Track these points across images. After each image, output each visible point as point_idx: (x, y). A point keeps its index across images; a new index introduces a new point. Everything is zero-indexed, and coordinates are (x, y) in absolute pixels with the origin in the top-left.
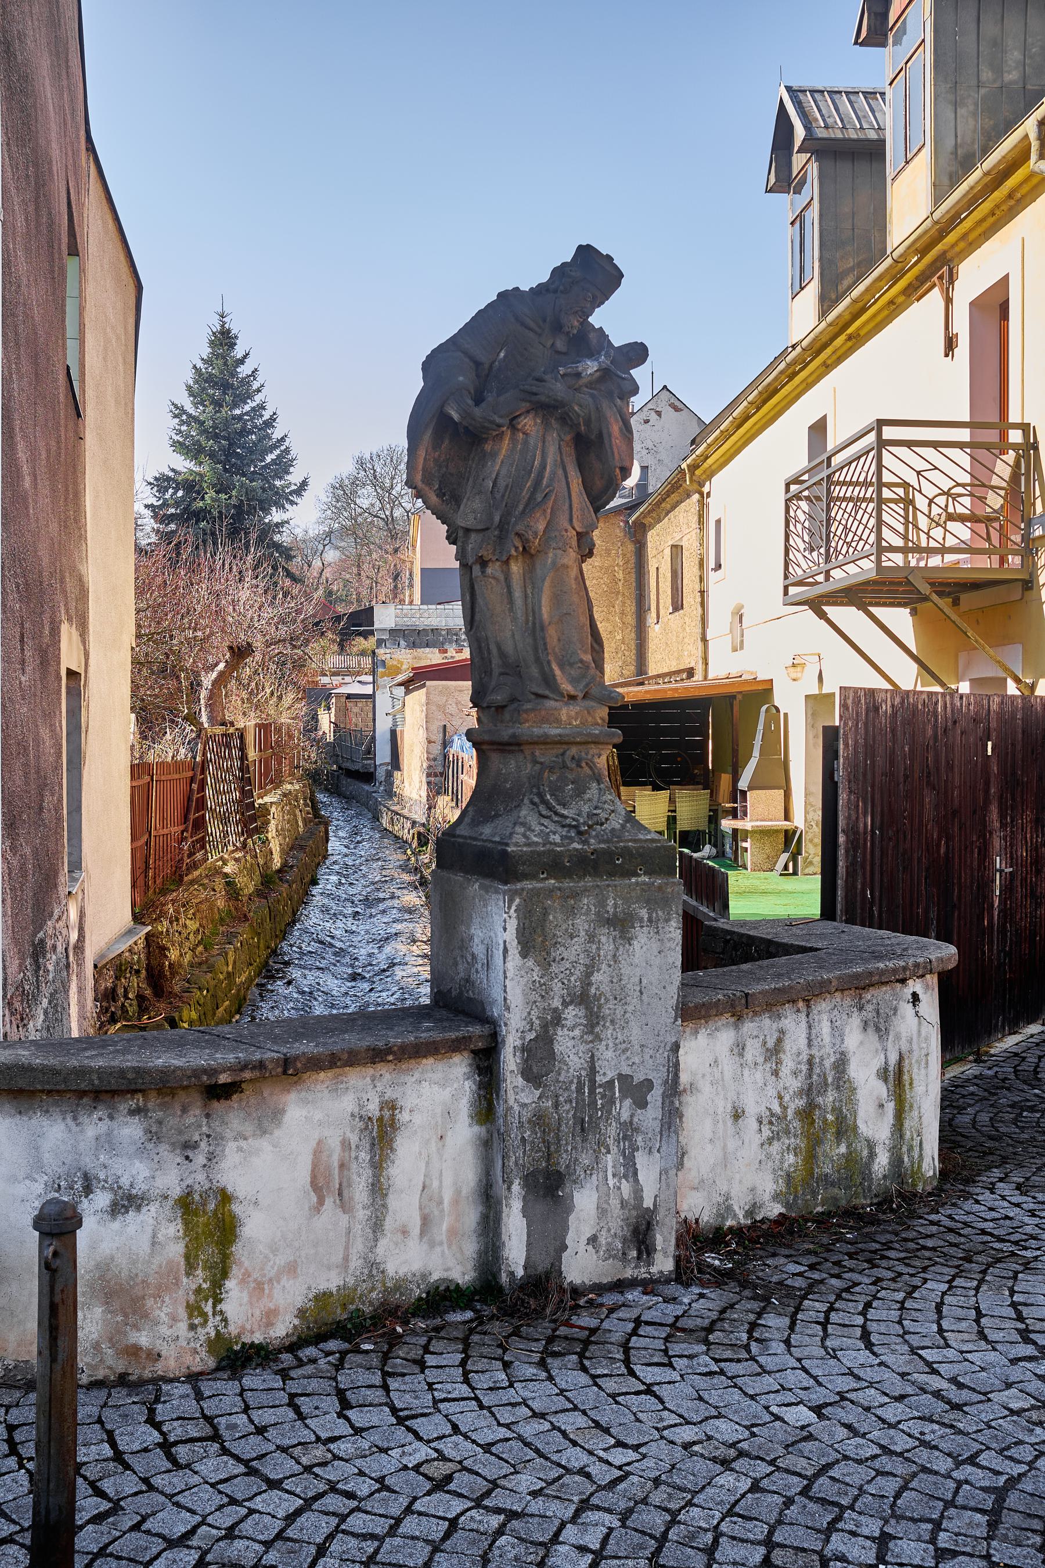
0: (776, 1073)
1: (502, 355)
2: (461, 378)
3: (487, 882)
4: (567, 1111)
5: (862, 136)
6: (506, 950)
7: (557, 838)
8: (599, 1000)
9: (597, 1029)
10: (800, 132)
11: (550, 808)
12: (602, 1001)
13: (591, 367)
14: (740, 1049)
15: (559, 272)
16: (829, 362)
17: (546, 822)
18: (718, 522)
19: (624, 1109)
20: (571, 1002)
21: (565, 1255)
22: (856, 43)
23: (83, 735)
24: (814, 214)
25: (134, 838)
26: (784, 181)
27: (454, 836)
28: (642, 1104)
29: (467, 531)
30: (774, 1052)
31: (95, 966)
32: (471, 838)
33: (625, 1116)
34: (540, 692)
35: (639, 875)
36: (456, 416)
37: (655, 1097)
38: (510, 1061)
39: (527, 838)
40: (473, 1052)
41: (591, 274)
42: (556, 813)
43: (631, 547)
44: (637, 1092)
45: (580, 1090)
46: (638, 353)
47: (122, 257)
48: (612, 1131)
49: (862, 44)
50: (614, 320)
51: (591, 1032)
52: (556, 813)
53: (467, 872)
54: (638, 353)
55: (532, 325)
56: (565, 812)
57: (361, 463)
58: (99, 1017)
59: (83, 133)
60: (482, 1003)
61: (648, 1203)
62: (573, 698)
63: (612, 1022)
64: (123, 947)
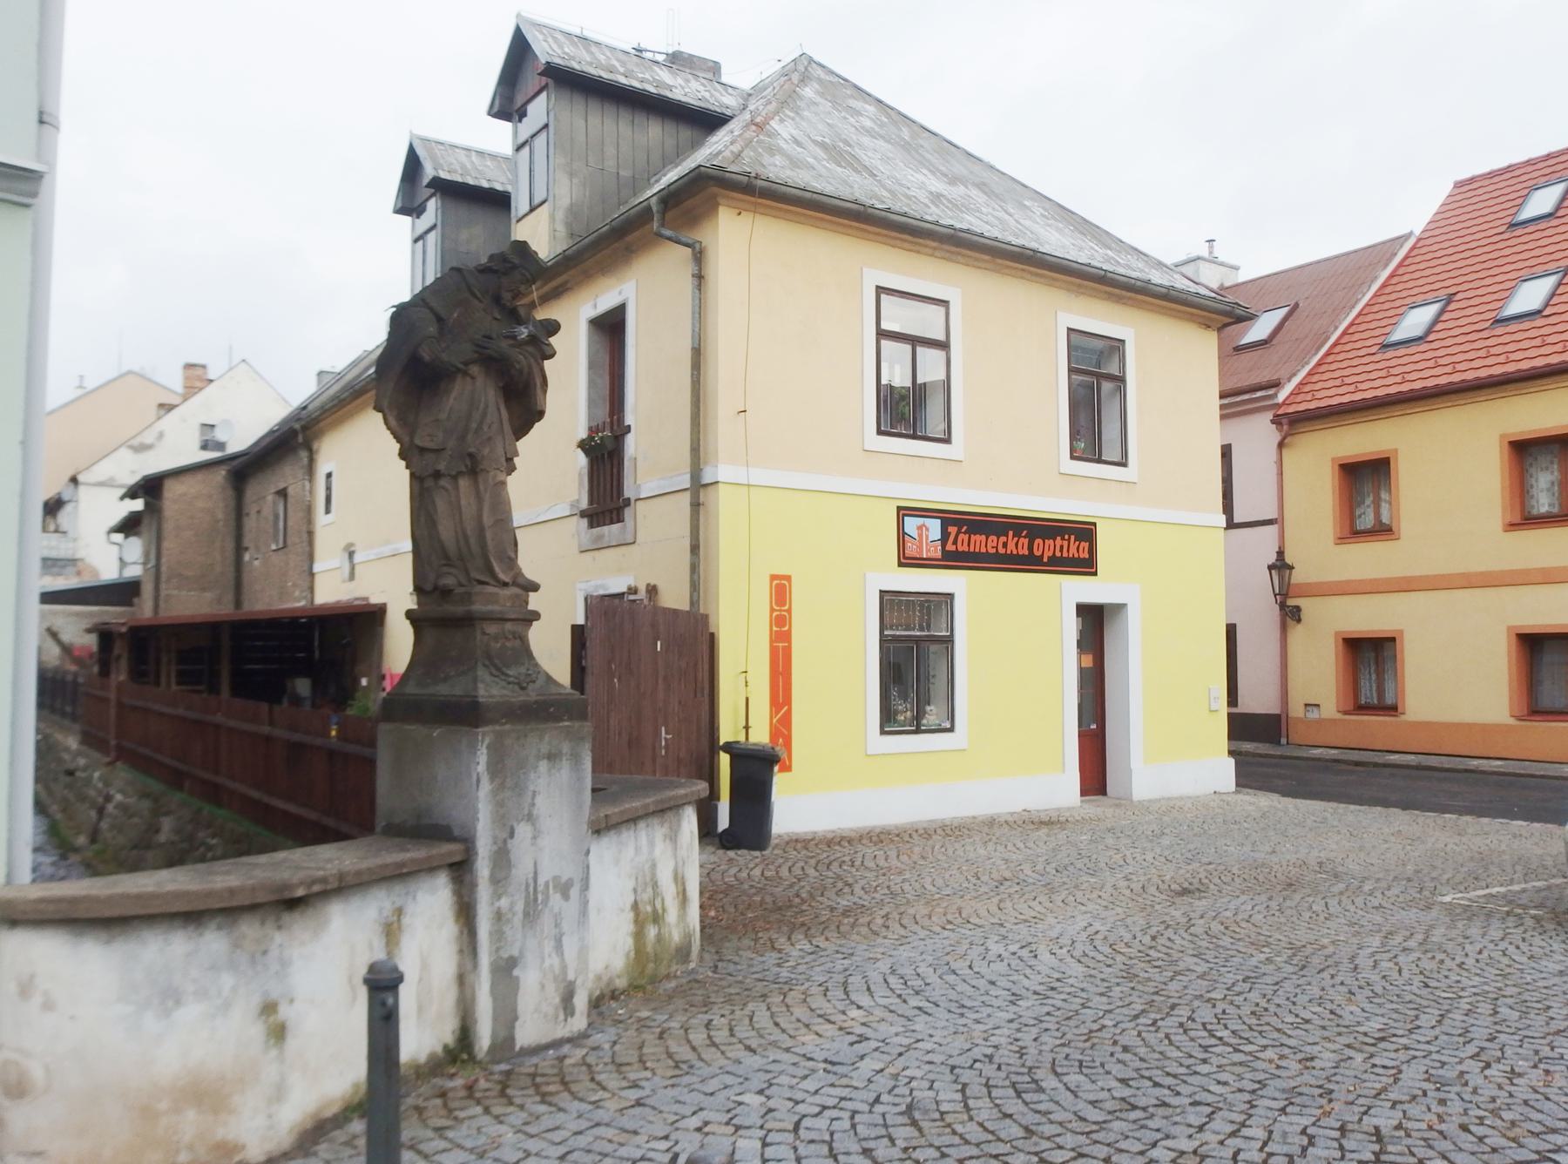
4: (520, 907)
6: (478, 781)
10: (429, 172)
11: (498, 669)
13: (524, 332)
18: (329, 475)
19: (556, 899)
21: (517, 1024)
24: (432, 238)
26: (409, 206)
28: (566, 896)
29: (422, 450)
33: (556, 910)
34: (482, 578)
37: (574, 892)
38: (483, 868)
43: (230, 493)
44: (564, 889)
45: (527, 886)
48: (546, 920)
61: (571, 977)
62: (505, 584)
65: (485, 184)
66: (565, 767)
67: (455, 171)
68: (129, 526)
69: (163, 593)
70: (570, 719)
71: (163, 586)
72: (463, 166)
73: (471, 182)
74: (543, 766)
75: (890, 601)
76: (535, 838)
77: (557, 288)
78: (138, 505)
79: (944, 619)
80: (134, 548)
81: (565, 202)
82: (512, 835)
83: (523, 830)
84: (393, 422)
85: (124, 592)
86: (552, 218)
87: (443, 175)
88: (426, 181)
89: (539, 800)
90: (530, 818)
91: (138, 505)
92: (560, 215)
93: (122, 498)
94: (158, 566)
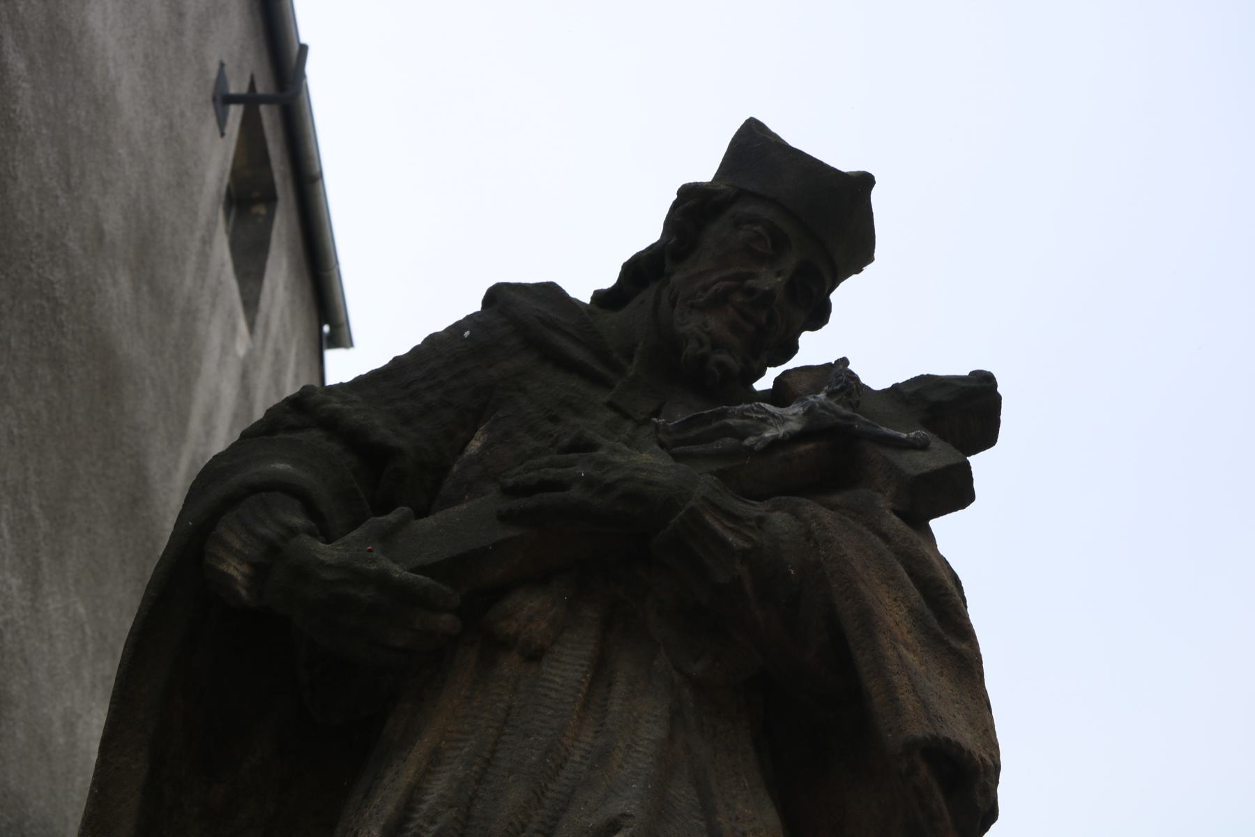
1: (475, 446)
2: (281, 466)
15: (692, 207)
36: (235, 570)
41: (777, 222)
46: (963, 411)
50: (873, 332)
54: (963, 411)
55: (578, 353)
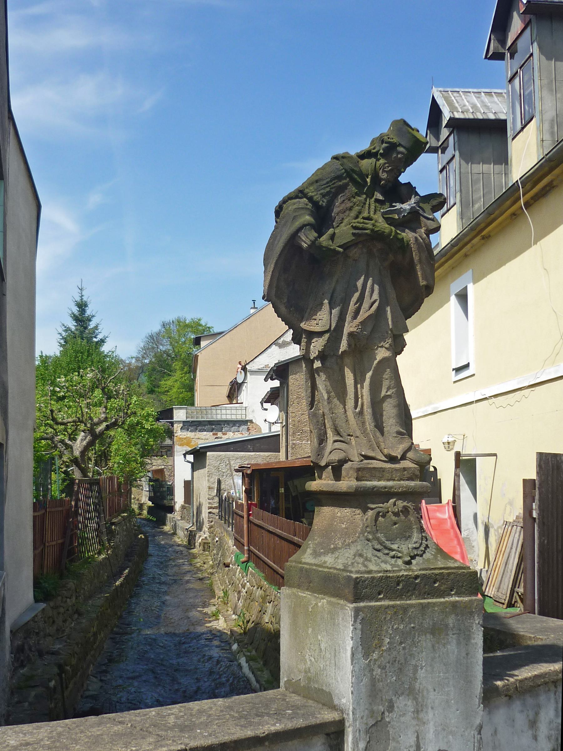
0: (535, 738)
3: (333, 600)
5: (485, 117)
7: (389, 568)
8: (423, 691)
9: (421, 715)
10: (447, 115)
12: (425, 693)
14: (512, 721)
16: (468, 253)
17: (379, 554)
20: (403, 694)
22: (486, 58)
23: (5, 484)
25: (35, 548)
27: (300, 563)
30: (533, 724)
31: (11, 631)
32: (315, 565)
35: (452, 595)
39: (366, 566)
40: (328, 735)
42: (386, 548)
47: (29, 187)
49: (489, 59)
51: (418, 719)
52: (386, 548)
53: (314, 592)
56: (395, 547)
57: (164, 325)
58: (13, 664)
59: (7, 109)
60: (330, 694)
63: (432, 708)
64: (28, 618)
65: (492, 117)
66: (452, 647)
67: (467, 111)
68: (272, 397)
69: (290, 442)
70: (458, 594)
71: (290, 438)
72: (474, 106)
73: (480, 117)
74: (426, 641)
75: (402, 126)
76: (417, 712)
77: (543, 188)
78: (276, 383)
79: (209, 341)
80: (273, 412)
81: (550, 114)
82: (391, 708)
83: (404, 704)
84: (283, 309)
85: (270, 443)
86: (540, 130)
87: (457, 115)
88: (444, 123)
89: (421, 673)
90: (411, 692)
91: (276, 383)
92: (546, 126)
93: (266, 380)
94: (287, 426)
